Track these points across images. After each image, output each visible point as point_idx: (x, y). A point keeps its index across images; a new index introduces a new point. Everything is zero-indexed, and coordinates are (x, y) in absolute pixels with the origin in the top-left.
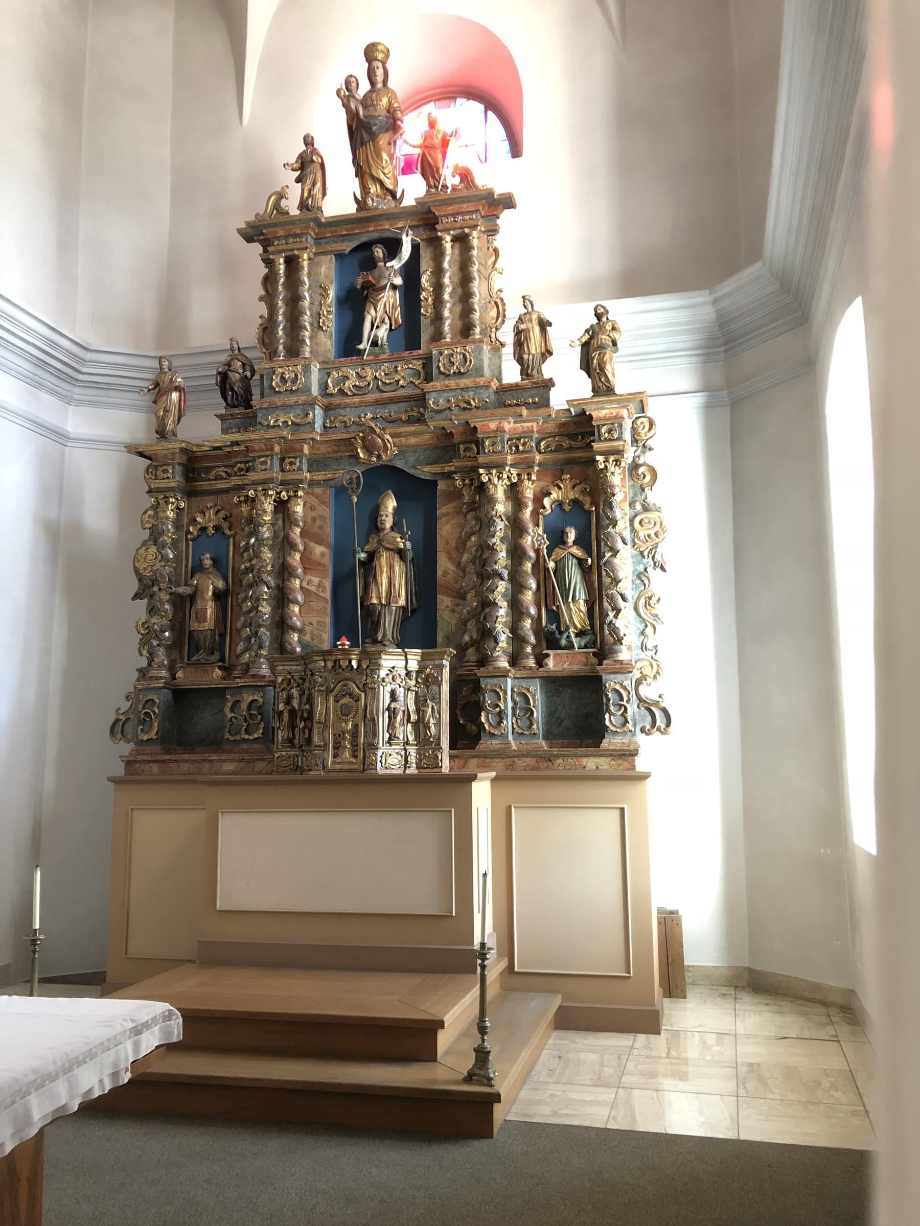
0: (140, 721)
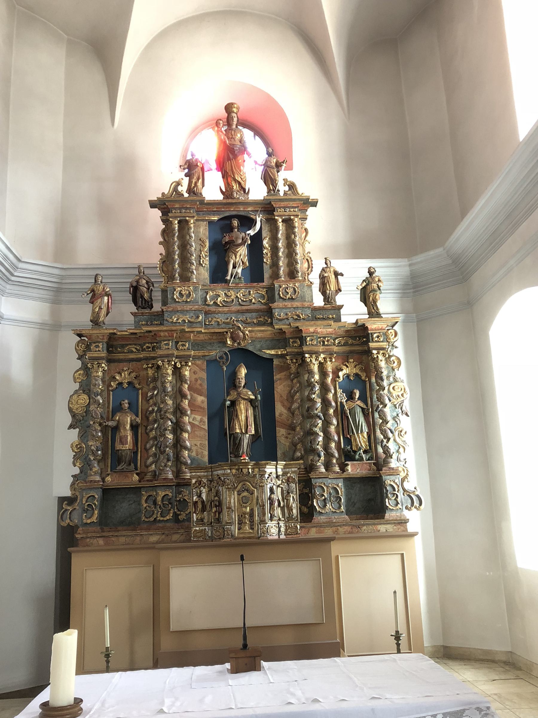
0: (84, 510)
